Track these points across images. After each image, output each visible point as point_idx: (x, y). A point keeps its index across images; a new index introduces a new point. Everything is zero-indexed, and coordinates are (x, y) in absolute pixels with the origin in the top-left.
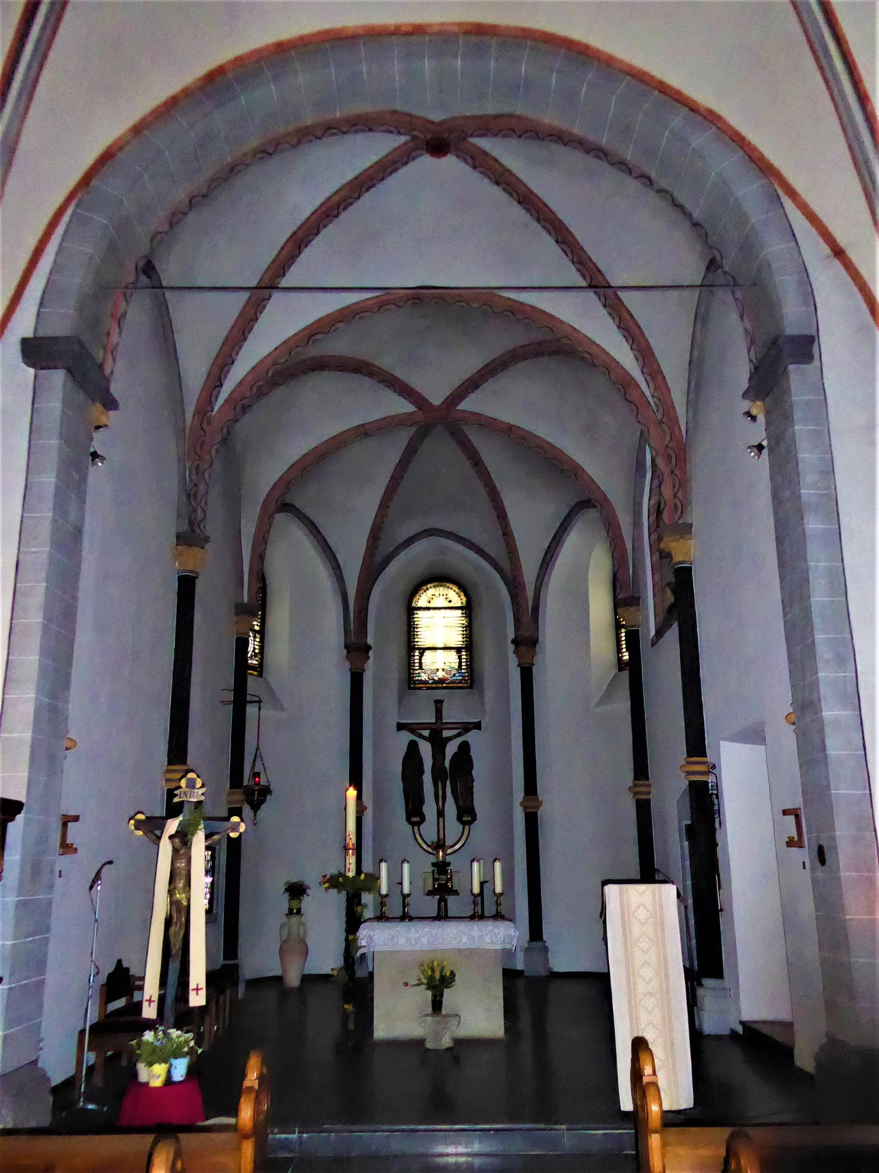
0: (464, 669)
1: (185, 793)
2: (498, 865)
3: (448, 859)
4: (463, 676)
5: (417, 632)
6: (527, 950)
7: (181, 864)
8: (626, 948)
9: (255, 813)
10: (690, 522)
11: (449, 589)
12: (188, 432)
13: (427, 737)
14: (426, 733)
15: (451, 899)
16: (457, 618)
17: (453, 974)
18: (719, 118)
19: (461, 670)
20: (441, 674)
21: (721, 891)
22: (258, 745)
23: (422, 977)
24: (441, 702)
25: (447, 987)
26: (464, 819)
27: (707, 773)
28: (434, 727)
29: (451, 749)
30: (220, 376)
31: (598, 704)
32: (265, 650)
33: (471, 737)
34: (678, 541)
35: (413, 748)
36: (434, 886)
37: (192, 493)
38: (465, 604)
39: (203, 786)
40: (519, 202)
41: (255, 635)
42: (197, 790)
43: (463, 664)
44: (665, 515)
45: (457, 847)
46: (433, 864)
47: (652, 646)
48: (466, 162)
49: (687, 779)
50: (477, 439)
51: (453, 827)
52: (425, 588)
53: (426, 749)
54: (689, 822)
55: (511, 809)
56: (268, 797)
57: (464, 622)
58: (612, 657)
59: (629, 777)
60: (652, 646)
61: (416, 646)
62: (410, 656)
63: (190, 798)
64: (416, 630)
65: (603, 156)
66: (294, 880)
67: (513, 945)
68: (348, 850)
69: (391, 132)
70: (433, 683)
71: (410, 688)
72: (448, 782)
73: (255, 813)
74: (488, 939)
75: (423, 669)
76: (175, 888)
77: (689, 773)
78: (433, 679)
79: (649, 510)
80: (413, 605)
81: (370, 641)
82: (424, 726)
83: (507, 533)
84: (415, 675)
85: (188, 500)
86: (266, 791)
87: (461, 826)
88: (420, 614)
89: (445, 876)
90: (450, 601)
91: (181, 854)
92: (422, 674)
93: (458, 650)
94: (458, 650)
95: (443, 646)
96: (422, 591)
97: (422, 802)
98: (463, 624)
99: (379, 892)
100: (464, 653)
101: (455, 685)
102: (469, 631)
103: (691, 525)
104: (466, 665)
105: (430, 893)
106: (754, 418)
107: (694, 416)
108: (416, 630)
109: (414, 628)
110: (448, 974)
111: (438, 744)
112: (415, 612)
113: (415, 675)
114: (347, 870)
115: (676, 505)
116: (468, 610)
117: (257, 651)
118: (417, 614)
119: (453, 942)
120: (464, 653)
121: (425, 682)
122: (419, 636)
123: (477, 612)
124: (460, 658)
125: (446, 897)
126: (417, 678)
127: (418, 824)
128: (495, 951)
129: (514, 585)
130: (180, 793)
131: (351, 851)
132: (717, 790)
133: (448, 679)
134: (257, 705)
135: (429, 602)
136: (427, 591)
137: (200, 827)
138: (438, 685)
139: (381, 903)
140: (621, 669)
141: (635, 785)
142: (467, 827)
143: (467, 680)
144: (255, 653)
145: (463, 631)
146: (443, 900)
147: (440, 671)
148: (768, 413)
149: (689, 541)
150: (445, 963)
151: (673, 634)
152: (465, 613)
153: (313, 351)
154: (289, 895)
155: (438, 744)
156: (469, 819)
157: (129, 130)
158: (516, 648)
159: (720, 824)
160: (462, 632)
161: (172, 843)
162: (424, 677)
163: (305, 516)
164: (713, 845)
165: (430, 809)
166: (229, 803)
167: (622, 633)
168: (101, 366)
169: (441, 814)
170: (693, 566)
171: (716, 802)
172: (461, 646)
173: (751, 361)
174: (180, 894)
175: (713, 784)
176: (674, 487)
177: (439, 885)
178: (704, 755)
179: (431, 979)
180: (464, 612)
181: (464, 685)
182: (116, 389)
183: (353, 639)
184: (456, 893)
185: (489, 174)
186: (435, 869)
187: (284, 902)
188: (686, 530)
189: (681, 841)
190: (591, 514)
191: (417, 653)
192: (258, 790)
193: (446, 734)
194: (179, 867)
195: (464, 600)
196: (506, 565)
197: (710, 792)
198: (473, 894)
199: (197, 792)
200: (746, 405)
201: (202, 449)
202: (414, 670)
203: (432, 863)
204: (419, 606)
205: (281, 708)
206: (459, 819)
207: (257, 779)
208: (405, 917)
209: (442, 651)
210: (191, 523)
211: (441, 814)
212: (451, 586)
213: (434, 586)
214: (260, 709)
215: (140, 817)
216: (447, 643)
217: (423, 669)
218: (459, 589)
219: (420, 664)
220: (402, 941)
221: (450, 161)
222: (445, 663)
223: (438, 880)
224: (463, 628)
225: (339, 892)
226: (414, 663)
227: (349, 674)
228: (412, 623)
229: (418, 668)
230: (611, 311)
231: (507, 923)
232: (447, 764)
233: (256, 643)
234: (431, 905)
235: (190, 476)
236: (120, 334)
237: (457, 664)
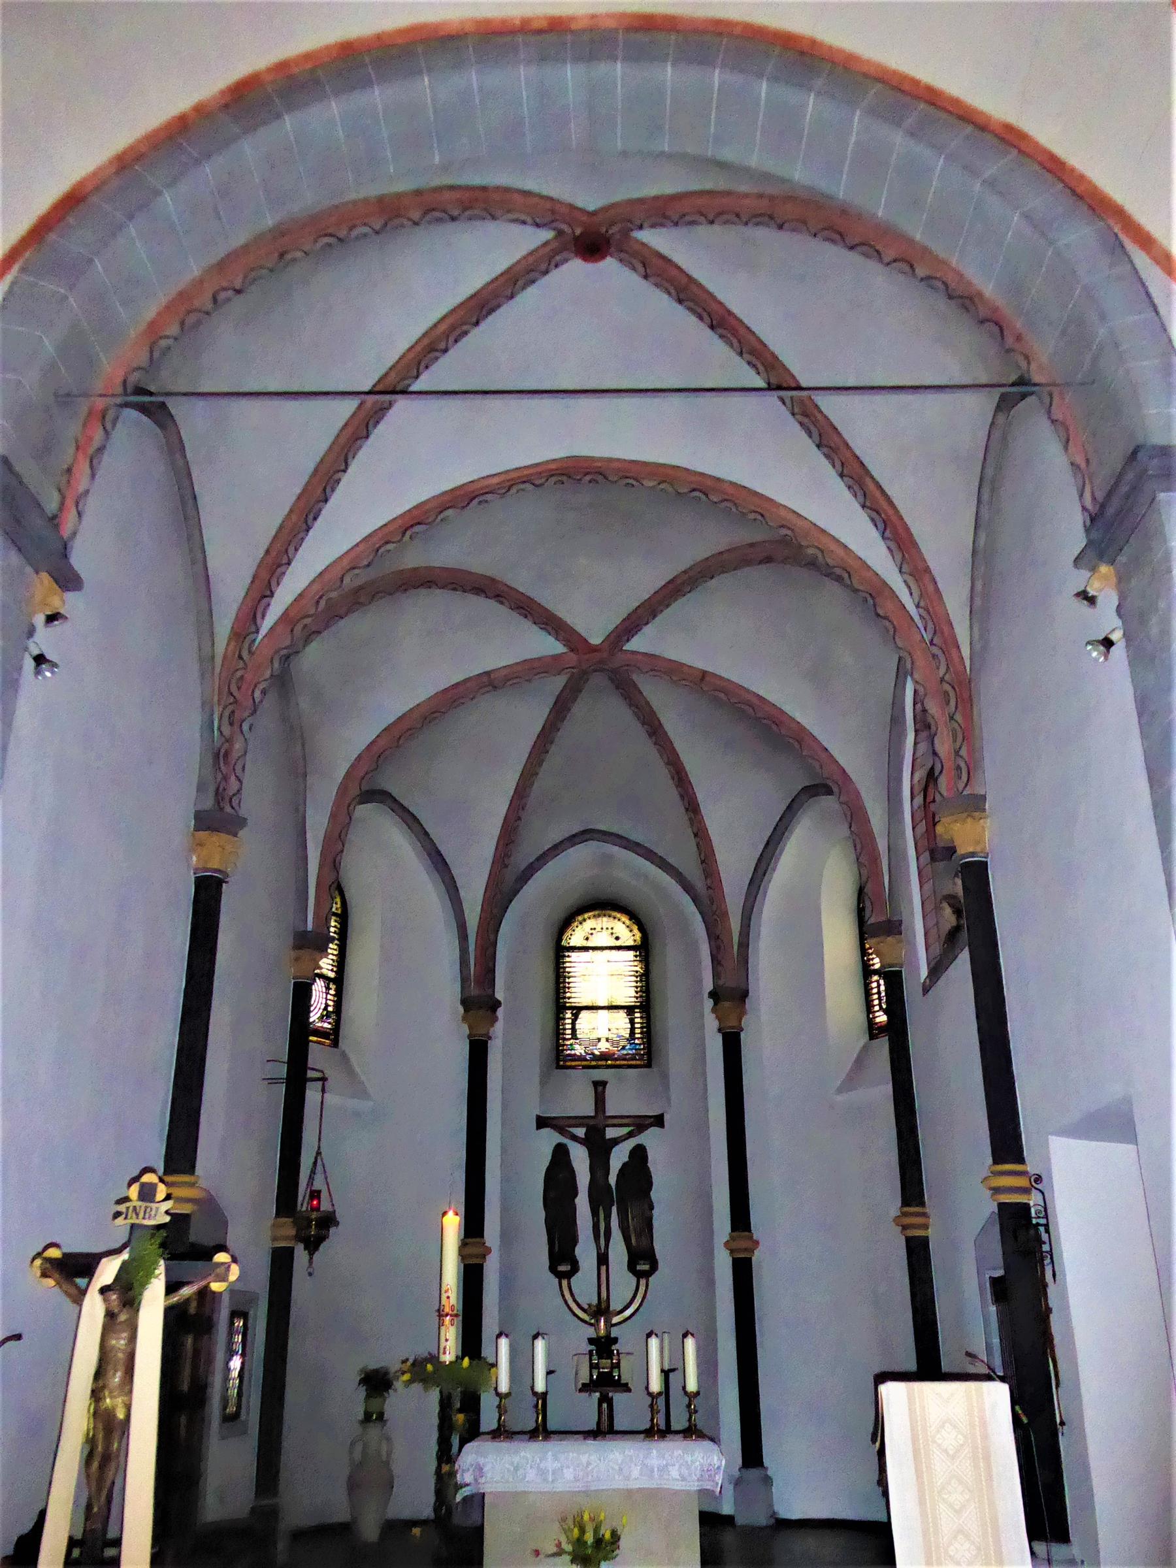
0: (638, 1038)
1: (135, 1208)
2: (690, 1343)
3: (614, 1332)
4: (636, 1050)
5: (569, 983)
6: (738, 1483)
7: (119, 1342)
8: (922, 1502)
9: (311, 1254)
10: (982, 793)
11: (616, 921)
12: (218, 661)
13: (582, 1139)
14: (580, 1132)
15: (618, 1398)
16: (627, 963)
17: (615, 1537)
18: (1022, 136)
19: (634, 1039)
20: (604, 1046)
21: (1059, 1389)
22: (319, 1147)
23: (563, 1539)
24: (604, 1084)
25: (606, 1559)
26: (639, 1268)
27: (1026, 1191)
28: (592, 1122)
29: (619, 1157)
30: (269, 582)
31: (840, 1091)
32: (344, 1007)
33: (649, 1139)
34: (964, 821)
35: (560, 1155)
36: (591, 1376)
37: (223, 751)
38: (639, 942)
39: (168, 1197)
40: (712, 327)
41: (328, 985)
42: (157, 1205)
43: (638, 1031)
44: (943, 782)
45: (628, 1313)
46: (591, 1341)
47: (924, 995)
48: (634, 269)
49: (994, 1200)
50: (654, 692)
51: (622, 1283)
52: (580, 918)
53: (580, 1158)
54: (1000, 1273)
55: (702, 1016)
56: (332, 1230)
57: (638, 969)
58: (861, 1018)
59: (894, 1205)
60: (924, 995)
61: (568, 1005)
62: (559, 1019)
63: (144, 1218)
64: (567, 980)
65: (837, 237)
66: (373, 1365)
67: (717, 1484)
68: (442, 1316)
69: (524, 223)
70: (592, 1060)
71: (559, 1067)
72: (614, 1209)
73: (311, 1254)
74: (674, 1473)
75: (577, 1039)
76: (104, 1387)
77: (996, 1190)
78: (593, 1054)
79: (912, 788)
80: (564, 943)
81: (499, 995)
82: (579, 1121)
83: (701, 834)
84: (565, 1047)
85: (214, 765)
86: (328, 1221)
87: (634, 1280)
88: (574, 956)
89: (609, 1361)
90: (617, 938)
91: (121, 1323)
92: (577, 1047)
93: (630, 1010)
94: (630, 1010)
95: (606, 1005)
96: (576, 924)
97: (574, 1241)
98: (637, 972)
99: (496, 1389)
100: (637, 1015)
101: (625, 1062)
102: (646, 983)
103: (984, 798)
104: (641, 1033)
105: (585, 1388)
106: (1091, 600)
107: (981, 636)
108: (567, 980)
109: (565, 977)
110: (608, 1536)
111: (600, 1149)
112: (567, 954)
113: (565, 1047)
114: (441, 1351)
115: (959, 768)
116: (644, 950)
117: (330, 1009)
118: (569, 956)
119: (617, 1477)
120: (637, 1015)
121: (581, 1058)
122: (572, 990)
123: (656, 950)
124: (632, 1022)
125: (610, 1394)
126: (569, 1052)
127: (569, 1275)
128: (688, 1492)
129: (714, 918)
130: (128, 1208)
131: (448, 1318)
132: (1046, 1217)
133: (614, 1054)
134: (320, 1083)
135: (587, 939)
136: (584, 923)
137: (157, 1272)
138: (600, 1063)
139: (499, 1407)
140: (872, 1037)
141: (904, 1214)
142: (643, 1282)
143: (643, 1055)
144: (328, 1012)
145: (637, 982)
146: (605, 1399)
147: (603, 1040)
148: (1122, 581)
149: (982, 821)
150: (602, 1517)
151: (962, 966)
152: (640, 955)
153: (414, 557)
154: (366, 1390)
155: (600, 1149)
156: (646, 1267)
157: (111, 162)
158: (716, 1004)
159: (1054, 1275)
160: (635, 984)
161: (105, 1300)
162: (579, 1050)
163: (405, 809)
164: (1043, 1316)
165: (586, 1252)
166: (274, 1239)
167: (872, 982)
168: (54, 521)
169: (603, 1259)
170: (989, 860)
171: (1045, 1237)
172: (633, 1004)
173: (1084, 508)
174: (111, 1398)
175: (1040, 1208)
176: (955, 741)
177: (600, 1374)
178: (1021, 1160)
179: (580, 1542)
180: (638, 953)
181: (638, 1062)
182: (79, 560)
183: (474, 991)
184: (626, 1388)
185: (667, 285)
186: (593, 1347)
187: (356, 1400)
188: (975, 805)
189: (984, 1306)
190: (828, 803)
191: (569, 1015)
192: (317, 1220)
193: (611, 1133)
194: (113, 1347)
195: (638, 936)
196: (699, 884)
197: (1034, 1221)
198: (650, 1394)
199: (157, 1209)
200: (1079, 579)
201: (239, 688)
202: (565, 1039)
203: (588, 1339)
204: (571, 944)
205: (363, 1094)
206: (632, 1267)
207: (315, 1203)
208: (541, 1432)
209: (607, 1011)
210: (219, 795)
211: (603, 1259)
212: (618, 915)
213: (594, 916)
214: (323, 1091)
215: (54, 1253)
216: (613, 1000)
217: (577, 1039)
218: (630, 920)
219: (574, 1029)
220: (531, 1475)
221: (609, 264)
222: (609, 1030)
223: (597, 1366)
224: (637, 977)
225: (426, 1389)
226: (565, 1029)
227: (468, 1041)
228: (562, 970)
229: (570, 1036)
230: (851, 482)
231: (707, 1444)
232: (613, 1180)
233: (329, 997)
234: (587, 1409)
235: (219, 729)
236: (93, 476)
237: (628, 1031)
